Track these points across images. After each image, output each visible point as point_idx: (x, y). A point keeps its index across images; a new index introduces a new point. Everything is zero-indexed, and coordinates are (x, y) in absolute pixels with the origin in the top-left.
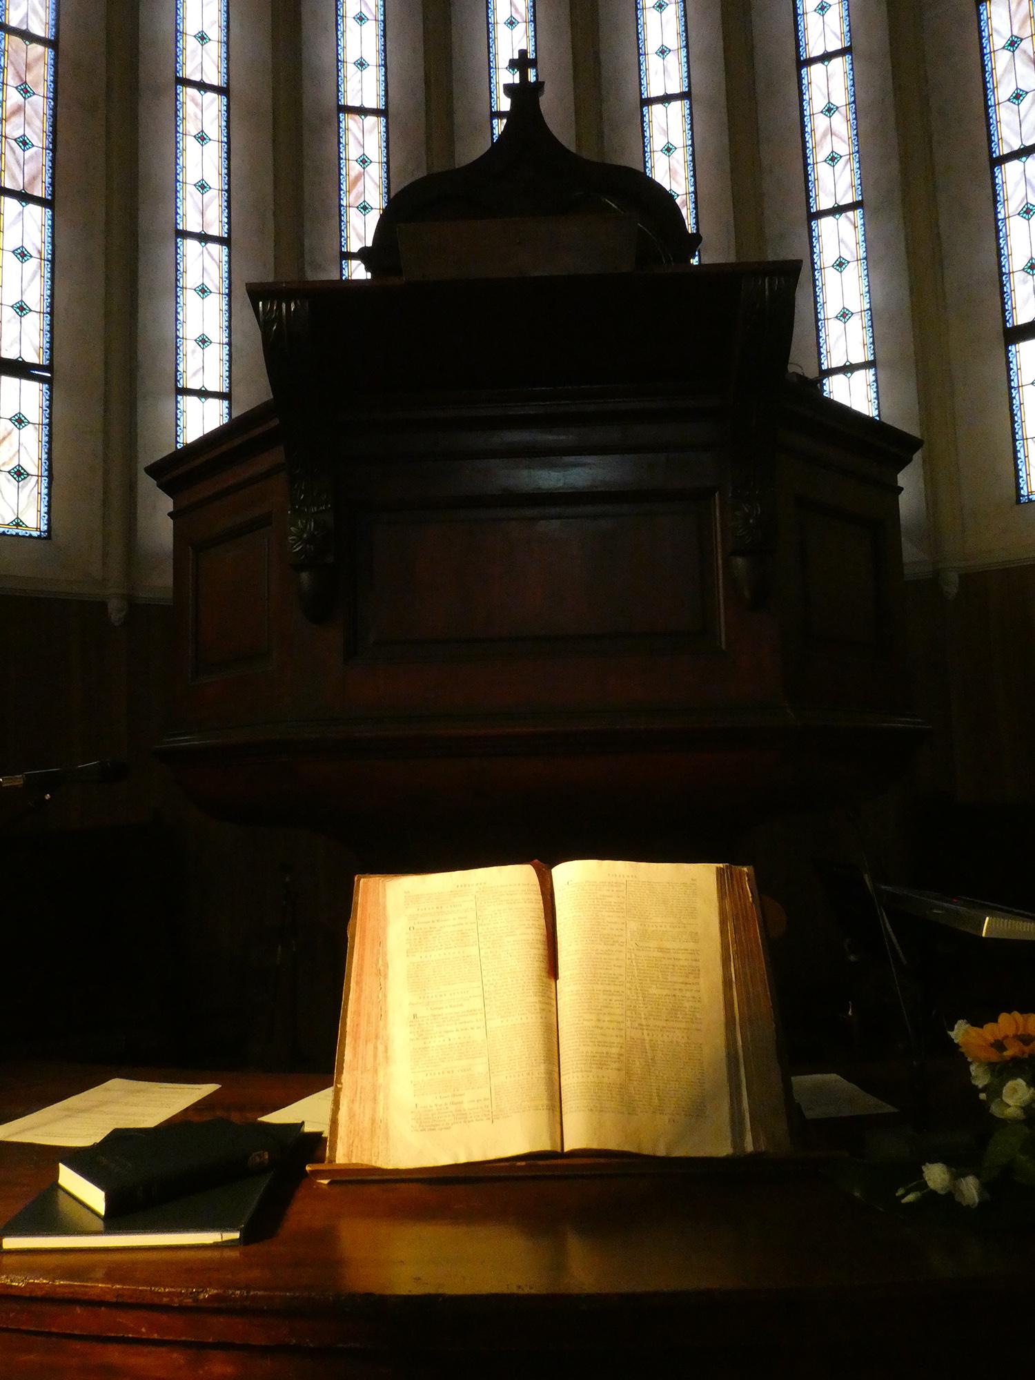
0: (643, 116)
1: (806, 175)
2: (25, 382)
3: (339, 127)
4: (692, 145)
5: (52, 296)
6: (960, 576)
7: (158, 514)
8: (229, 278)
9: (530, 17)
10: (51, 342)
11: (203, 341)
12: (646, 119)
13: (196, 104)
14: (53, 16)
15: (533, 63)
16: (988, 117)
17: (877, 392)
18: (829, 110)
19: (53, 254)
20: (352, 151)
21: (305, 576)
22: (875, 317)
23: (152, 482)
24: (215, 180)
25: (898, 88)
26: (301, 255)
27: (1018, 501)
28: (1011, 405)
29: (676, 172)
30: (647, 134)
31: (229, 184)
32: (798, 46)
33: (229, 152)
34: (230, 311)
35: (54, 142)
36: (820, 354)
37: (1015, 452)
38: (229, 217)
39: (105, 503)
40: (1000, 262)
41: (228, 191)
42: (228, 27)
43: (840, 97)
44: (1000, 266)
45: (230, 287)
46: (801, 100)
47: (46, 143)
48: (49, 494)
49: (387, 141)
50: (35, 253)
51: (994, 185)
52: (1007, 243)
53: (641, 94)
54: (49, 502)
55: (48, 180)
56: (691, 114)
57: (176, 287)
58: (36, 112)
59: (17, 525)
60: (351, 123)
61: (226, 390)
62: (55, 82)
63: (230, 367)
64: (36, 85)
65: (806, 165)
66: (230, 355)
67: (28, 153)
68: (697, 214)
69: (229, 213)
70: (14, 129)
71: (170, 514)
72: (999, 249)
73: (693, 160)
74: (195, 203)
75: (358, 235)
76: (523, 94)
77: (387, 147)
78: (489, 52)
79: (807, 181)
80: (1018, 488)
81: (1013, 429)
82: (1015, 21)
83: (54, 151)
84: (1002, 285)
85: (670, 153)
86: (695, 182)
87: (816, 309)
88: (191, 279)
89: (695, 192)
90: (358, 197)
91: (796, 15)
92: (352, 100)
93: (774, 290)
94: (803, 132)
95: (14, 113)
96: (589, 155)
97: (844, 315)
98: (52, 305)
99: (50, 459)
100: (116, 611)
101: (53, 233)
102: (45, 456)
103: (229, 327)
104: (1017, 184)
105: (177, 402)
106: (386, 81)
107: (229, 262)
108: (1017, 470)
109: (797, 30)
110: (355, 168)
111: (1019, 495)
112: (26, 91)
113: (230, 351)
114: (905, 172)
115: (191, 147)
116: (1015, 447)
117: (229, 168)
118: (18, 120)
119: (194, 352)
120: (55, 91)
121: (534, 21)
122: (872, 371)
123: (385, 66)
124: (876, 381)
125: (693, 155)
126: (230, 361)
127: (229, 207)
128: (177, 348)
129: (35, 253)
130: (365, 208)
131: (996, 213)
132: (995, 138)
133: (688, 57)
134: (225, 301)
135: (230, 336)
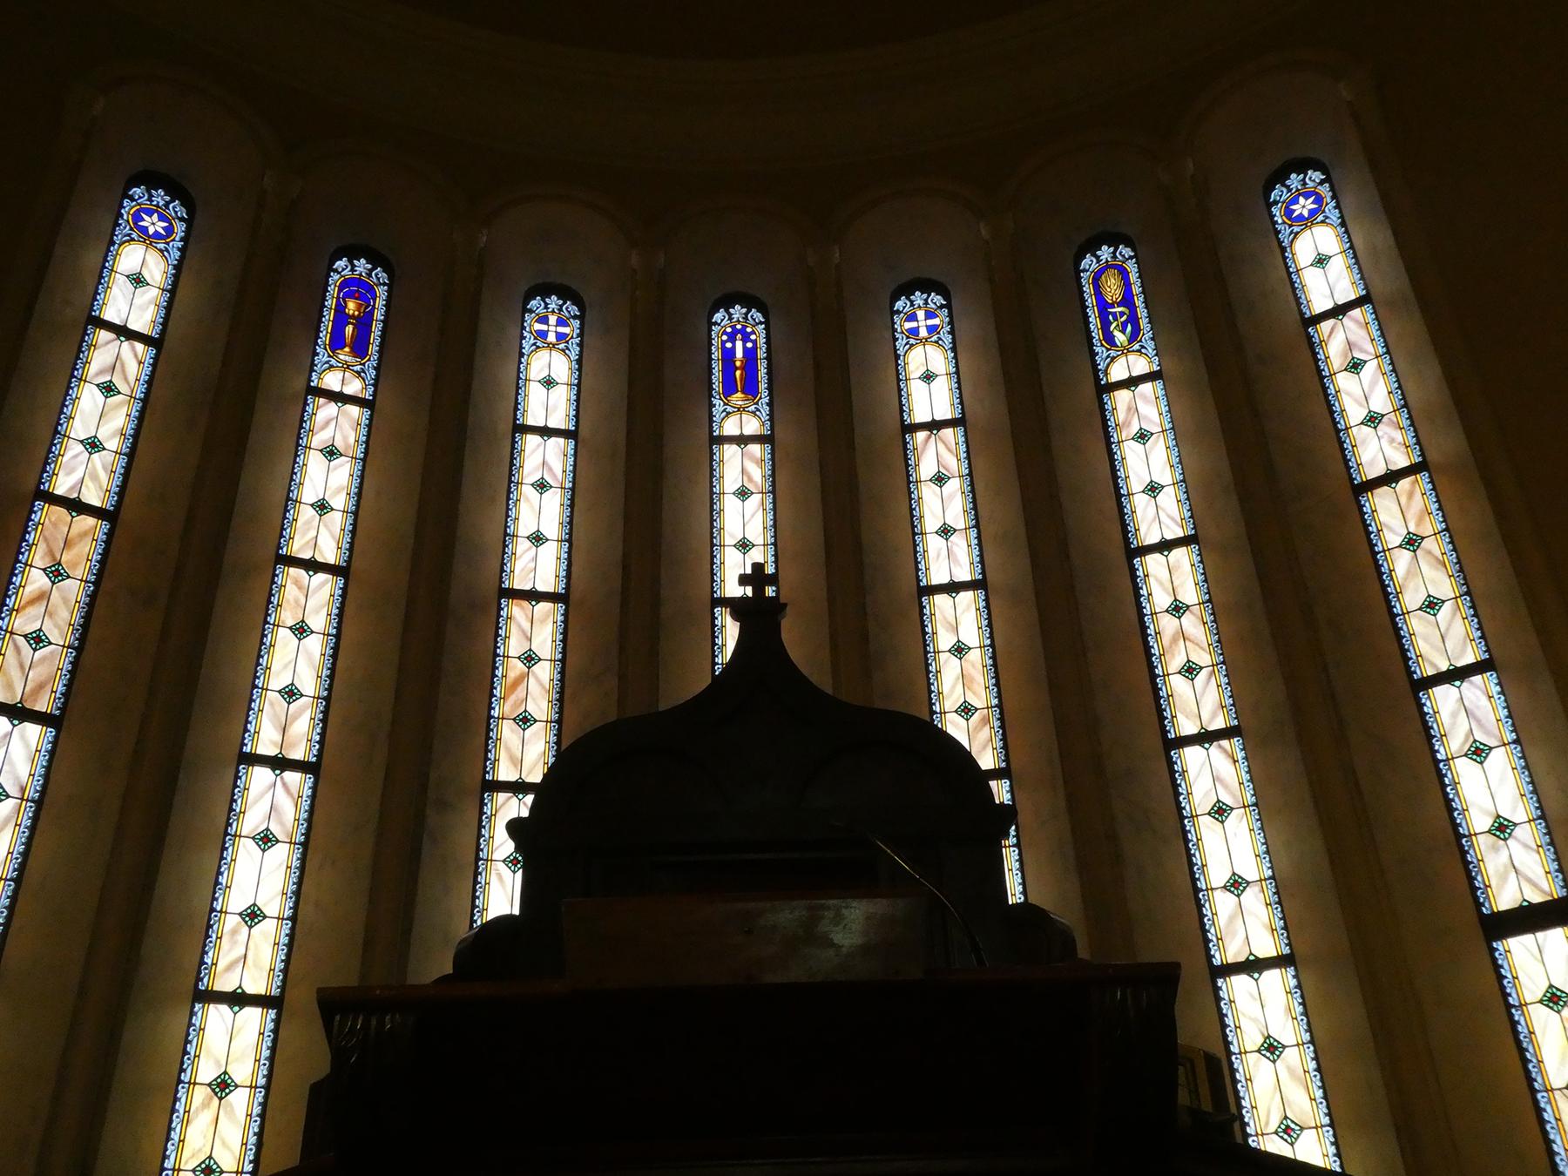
0: (922, 607)
3: (499, 616)
4: (992, 645)
9: (767, 486)
12: (927, 611)
13: (300, 588)
15: (773, 580)
17: (1303, 1004)
18: (1177, 609)
20: (514, 646)
29: (972, 680)
30: (929, 630)
32: (1125, 532)
34: (302, 868)
35: (82, 639)
43: (1190, 594)
45: (307, 835)
46: (1138, 596)
51: (1423, 715)
52: (1457, 793)
53: (919, 581)
55: (61, 689)
56: (988, 607)
60: (517, 611)
63: (288, 955)
64: (75, 565)
68: (1004, 734)
69: (324, 729)
70: (25, 623)
73: (995, 665)
74: (276, 715)
75: (512, 758)
77: (564, 641)
78: (712, 527)
79: (1157, 697)
82: (1409, 516)
85: (963, 692)
86: (999, 692)
87: (1192, 873)
88: (252, 820)
89: (1000, 706)
90: (516, 705)
91: (1119, 496)
94: (1145, 636)
101: (50, 761)
103: (297, 894)
104: (1454, 715)
106: (569, 559)
109: (1122, 514)
110: (517, 667)
112: (57, 574)
113: (293, 929)
121: (773, 492)
123: (570, 541)
124: (1299, 986)
125: (994, 657)
126: (290, 946)
127: (324, 721)
128: (210, 926)
132: (1411, 654)
133: (979, 537)
135: (296, 908)
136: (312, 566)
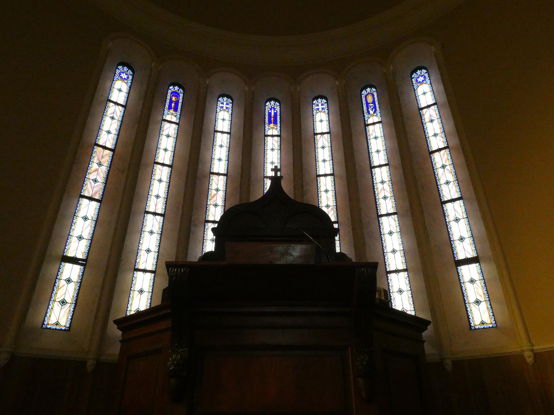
0: (317, 180)
1: (376, 202)
2: (75, 266)
4: (335, 190)
5: (93, 234)
6: (452, 361)
7: (116, 332)
8: (162, 228)
10: (89, 250)
11: (148, 251)
14: (119, 128)
15: (280, 170)
16: (438, 189)
19: (97, 219)
20: (213, 186)
21: (173, 380)
22: (405, 253)
23: (116, 326)
24: (163, 194)
25: (406, 178)
26: (190, 221)
27: (471, 329)
28: (462, 289)
31: (167, 196)
32: (370, 162)
33: (169, 186)
35: (106, 181)
36: (386, 265)
37: (466, 308)
38: (165, 207)
39: (96, 317)
40: (449, 237)
41: (167, 198)
42: (175, 147)
44: (450, 238)
45: (162, 232)
46: (373, 179)
47: (103, 181)
48: (73, 311)
49: (226, 184)
50: (90, 218)
54: (73, 314)
55: (101, 193)
57: (141, 231)
58: (102, 171)
59: (57, 324)
60: (214, 178)
61: (154, 270)
62: (111, 162)
63: (157, 261)
64: (104, 163)
65: (376, 199)
66: (158, 256)
67: (96, 184)
71: (120, 341)
72: (448, 232)
75: (213, 215)
76: (275, 180)
77: (226, 186)
79: (376, 204)
80: (470, 323)
81: (464, 299)
83: (106, 184)
84: (452, 245)
85: (327, 200)
88: (147, 228)
89: (336, 205)
90: (214, 202)
91: (369, 153)
92: (215, 170)
93: (368, 274)
94: (374, 189)
95: (94, 171)
96: (298, 200)
97: (394, 251)
98: (92, 237)
99: (77, 296)
100: (90, 365)
102: (76, 295)
103: (159, 246)
105: (134, 274)
107: (163, 223)
108: (468, 316)
109: (370, 158)
110: (214, 192)
111: (470, 326)
114: (411, 205)
115: (155, 184)
116: (466, 306)
117: (168, 191)
118: (96, 173)
119: (144, 255)
120: (111, 165)
122: (406, 273)
124: (408, 276)
125: (335, 193)
126: (157, 258)
127: (166, 204)
129: (90, 218)
130: (216, 205)
131: (446, 220)
134: (159, 236)
135: (159, 249)
136: (163, 165)
